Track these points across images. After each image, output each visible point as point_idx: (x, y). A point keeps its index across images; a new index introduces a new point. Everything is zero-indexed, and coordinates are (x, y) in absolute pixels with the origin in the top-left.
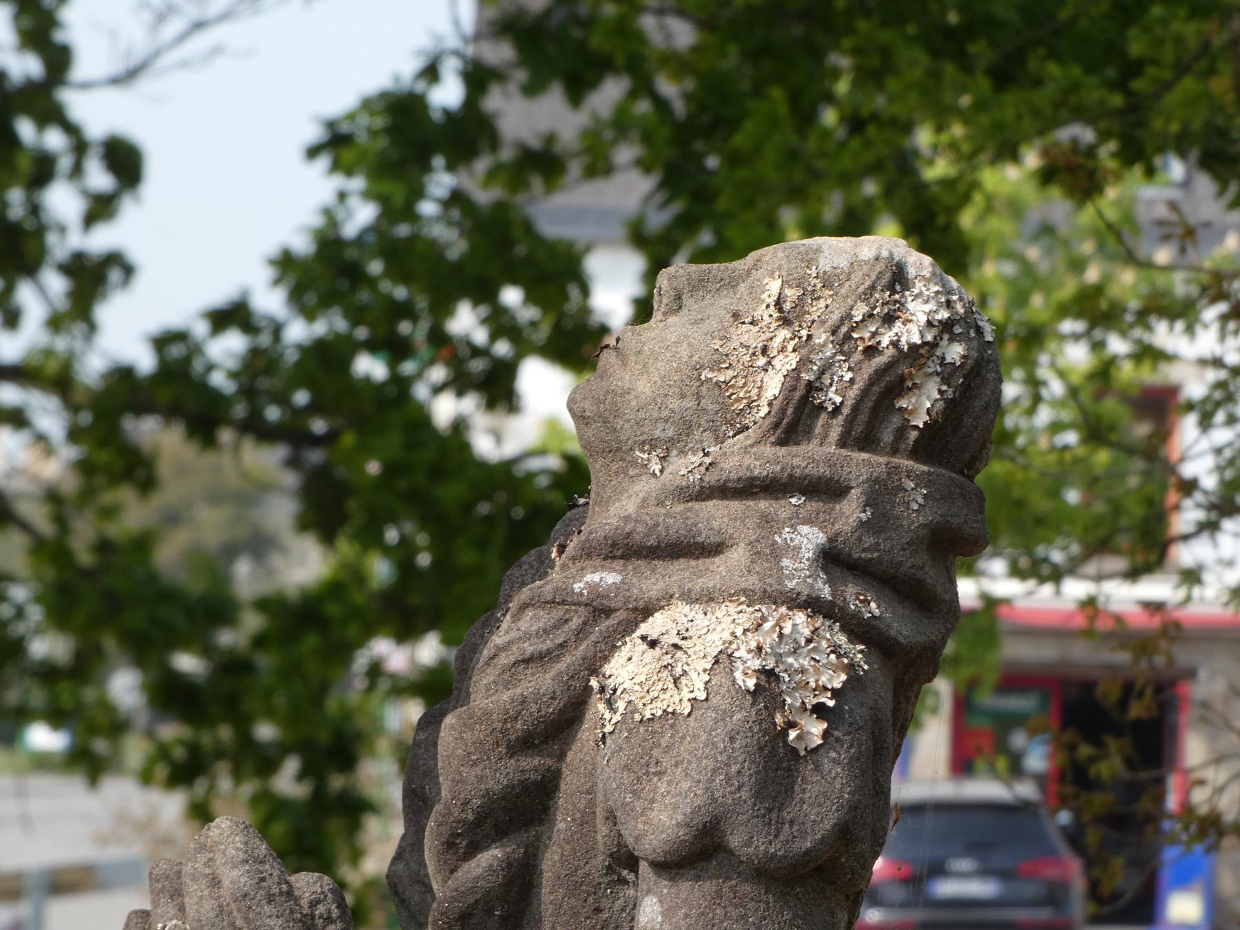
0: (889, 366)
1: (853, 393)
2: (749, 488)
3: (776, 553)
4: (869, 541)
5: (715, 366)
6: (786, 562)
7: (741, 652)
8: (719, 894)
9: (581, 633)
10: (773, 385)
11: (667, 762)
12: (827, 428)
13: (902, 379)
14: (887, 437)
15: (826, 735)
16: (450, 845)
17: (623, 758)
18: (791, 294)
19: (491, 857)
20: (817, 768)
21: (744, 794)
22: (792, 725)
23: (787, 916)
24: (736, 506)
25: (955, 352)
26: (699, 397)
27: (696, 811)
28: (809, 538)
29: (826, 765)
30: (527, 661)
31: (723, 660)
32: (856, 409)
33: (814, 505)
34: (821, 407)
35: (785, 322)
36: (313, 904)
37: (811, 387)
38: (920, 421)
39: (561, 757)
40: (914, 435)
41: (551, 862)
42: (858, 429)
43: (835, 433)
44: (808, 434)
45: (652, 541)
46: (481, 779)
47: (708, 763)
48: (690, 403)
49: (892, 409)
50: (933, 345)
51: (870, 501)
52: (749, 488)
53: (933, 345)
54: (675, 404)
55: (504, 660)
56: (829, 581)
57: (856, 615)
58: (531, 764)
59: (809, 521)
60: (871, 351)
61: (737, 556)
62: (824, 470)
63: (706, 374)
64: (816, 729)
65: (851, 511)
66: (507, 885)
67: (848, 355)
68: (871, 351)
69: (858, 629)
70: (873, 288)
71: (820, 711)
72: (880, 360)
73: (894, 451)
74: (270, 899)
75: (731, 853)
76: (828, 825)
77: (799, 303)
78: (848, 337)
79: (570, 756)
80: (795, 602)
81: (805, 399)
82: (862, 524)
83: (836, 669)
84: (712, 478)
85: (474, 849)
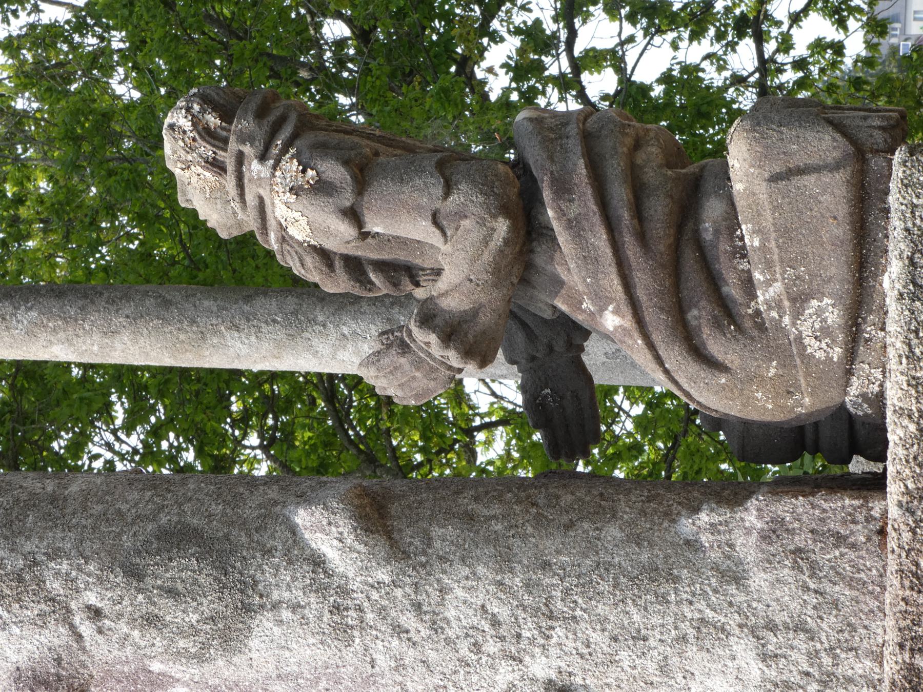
0: (199, 134)
1: (207, 146)
2: (240, 186)
3: (260, 179)
4: (257, 143)
5: (205, 193)
6: (262, 176)
7: (285, 198)
8: (368, 208)
9: (292, 247)
10: (208, 174)
11: (324, 225)
12: (220, 156)
13: (204, 128)
14: (224, 133)
15: (312, 169)
16: (370, 290)
17: (325, 239)
18: (179, 165)
19: (372, 276)
20: (324, 172)
21: (331, 201)
22: (308, 182)
23: (376, 183)
24: (247, 190)
25: (196, 107)
26: (216, 198)
27: (337, 217)
28: (255, 166)
29: (323, 169)
30: (303, 265)
31: (288, 205)
32: (214, 146)
33: (246, 163)
34: (214, 158)
35: (189, 167)
36: (383, 344)
37: (207, 162)
38: (218, 122)
39: (335, 253)
40: (223, 124)
41: (375, 256)
42: (221, 145)
43: (223, 153)
44: (223, 162)
45: (259, 221)
46: (343, 282)
47: (321, 213)
48: (218, 201)
49: (215, 132)
50: (193, 116)
51: (243, 142)
52: (240, 186)
53: (193, 116)
54: (219, 206)
55: (303, 271)
56: (268, 159)
57: (280, 151)
58: (338, 264)
59: (250, 165)
60: (194, 140)
61: (262, 192)
62: (233, 159)
63: (208, 196)
64: (310, 173)
65: (247, 149)
66: (382, 271)
67: (196, 148)
68: (194, 140)
69: (284, 151)
70: (174, 138)
71: (304, 171)
72: (197, 137)
73: (229, 131)
74: (379, 361)
75: (353, 204)
76: (342, 170)
77: (182, 162)
78: (190, 148)
79: (335, 250)
80: (273, 175)
81: (211, 164)
82: (251, 146)
83: (292, 163)
84: (237, 199)
85: (371, 282)
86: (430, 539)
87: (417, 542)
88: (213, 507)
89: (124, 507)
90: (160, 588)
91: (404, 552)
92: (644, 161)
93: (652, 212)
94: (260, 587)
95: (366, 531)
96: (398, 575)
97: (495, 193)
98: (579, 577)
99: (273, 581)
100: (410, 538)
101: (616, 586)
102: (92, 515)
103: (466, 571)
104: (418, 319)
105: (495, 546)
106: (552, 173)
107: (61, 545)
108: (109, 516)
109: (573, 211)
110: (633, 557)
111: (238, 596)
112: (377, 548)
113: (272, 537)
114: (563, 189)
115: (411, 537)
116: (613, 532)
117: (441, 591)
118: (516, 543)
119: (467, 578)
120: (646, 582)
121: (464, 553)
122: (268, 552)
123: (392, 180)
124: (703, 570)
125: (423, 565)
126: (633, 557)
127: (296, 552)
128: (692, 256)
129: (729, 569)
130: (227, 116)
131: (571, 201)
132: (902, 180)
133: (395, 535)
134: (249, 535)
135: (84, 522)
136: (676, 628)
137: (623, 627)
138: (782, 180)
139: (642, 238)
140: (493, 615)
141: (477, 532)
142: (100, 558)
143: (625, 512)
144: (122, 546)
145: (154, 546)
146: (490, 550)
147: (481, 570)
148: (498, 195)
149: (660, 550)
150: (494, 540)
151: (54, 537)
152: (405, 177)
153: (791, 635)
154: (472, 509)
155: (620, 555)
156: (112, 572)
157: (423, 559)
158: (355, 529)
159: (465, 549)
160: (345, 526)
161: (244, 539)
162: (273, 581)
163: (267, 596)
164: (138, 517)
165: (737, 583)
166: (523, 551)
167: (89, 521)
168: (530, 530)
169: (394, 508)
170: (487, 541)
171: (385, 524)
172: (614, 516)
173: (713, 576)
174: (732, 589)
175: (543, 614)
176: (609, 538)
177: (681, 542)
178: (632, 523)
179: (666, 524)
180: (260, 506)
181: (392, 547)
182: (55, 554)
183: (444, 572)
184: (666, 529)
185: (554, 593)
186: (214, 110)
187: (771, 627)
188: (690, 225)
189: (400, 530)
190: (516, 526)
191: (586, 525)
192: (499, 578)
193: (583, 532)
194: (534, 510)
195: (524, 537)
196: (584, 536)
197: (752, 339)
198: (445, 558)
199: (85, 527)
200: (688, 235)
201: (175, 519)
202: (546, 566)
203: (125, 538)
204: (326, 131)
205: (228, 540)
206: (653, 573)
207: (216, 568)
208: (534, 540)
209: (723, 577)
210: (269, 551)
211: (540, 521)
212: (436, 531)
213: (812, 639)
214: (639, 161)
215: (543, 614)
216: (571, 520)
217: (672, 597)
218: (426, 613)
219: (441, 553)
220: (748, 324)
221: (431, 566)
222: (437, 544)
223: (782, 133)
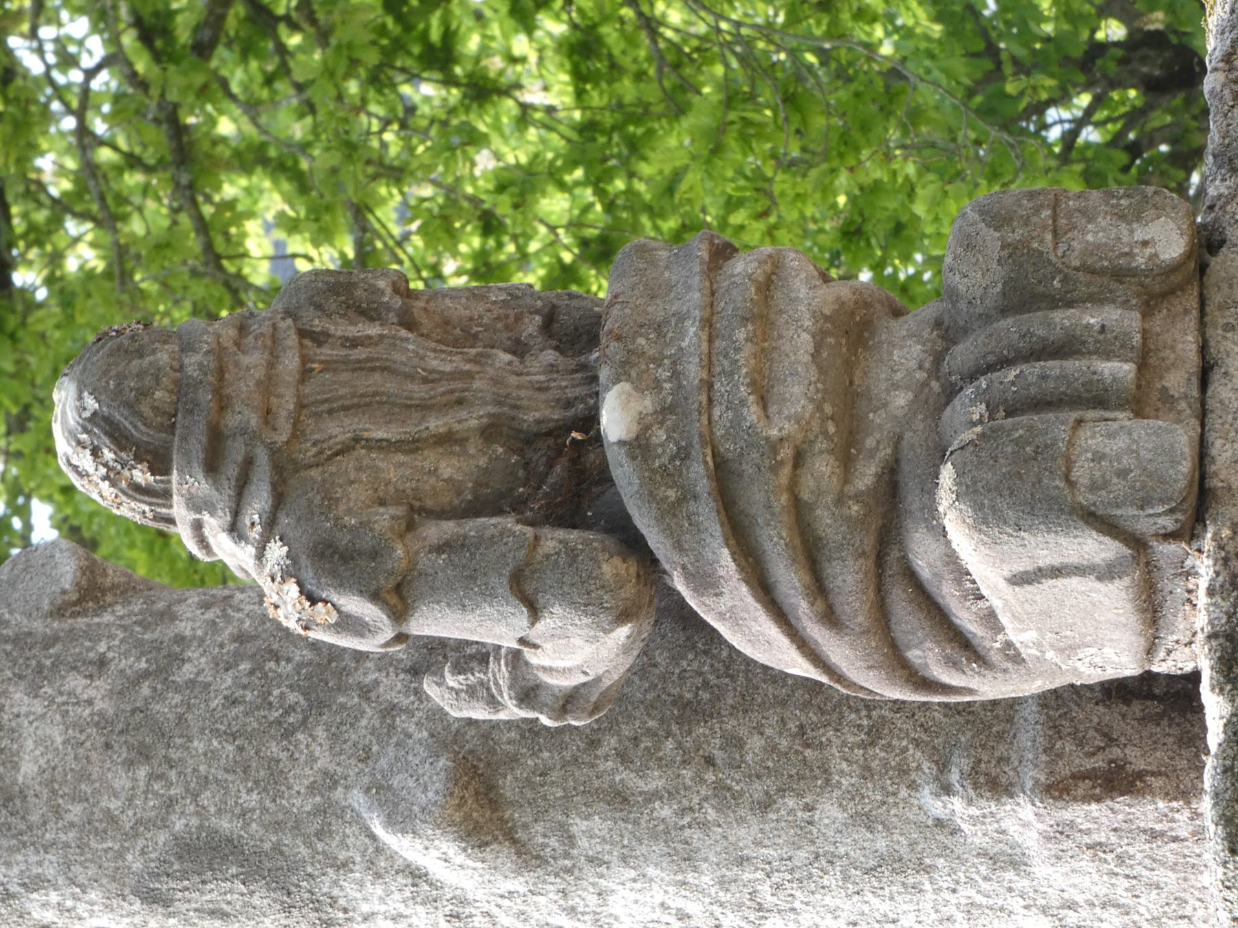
4: (220, 513)
40: (158, 478)
86: (571, 837)
87: (553, 842)
88: (244, 795)
89: (114, 805)
90: (196, 910)
91: (537, 857)
92: (812, 492)
93: (839, 582)
94: (342, 902)
95: (480, 847)
96: (535, 884)
97: (607, 608)
98: (792, 871)
99: (359, 895)
100: (539, 835)
101: (846, 879)
102: (72, 825)
103: (633, 874)
104: (513, 694)
105: (666, 842)
106: (684, 567)
107: (40, 870)
108: (97, 824)
109: (725, 602)
110: (865, 844)
111: (314, 915)
112: (499, 860)
113: (343, 844)
114: (705, 582)
115: (545, 836)
116: (830, 812)
117: (600, 894)
118: (695, 835)
119: (634, 881)
120: (886, 873)
121: (625, 851)
122: (344, 866)
123: (449, 605)
124: (965, 856)
125: (569, 871)
126: (865, 844)
127: (383, 864)
128: (904, 596)
129: (1003, 853)
130: (160, 465)
131: (720, 594)
132: (1223, 883)
133: (520, 835)
134: (310, 845)
135: (63, 838)
136: (937, 911)
137: (863, 914)
138: (1030, 583)
139: (830, 618)
140: (679, 910)
141: (636, 822)
142: (101, 885)
143: (842, 773)
144: (129, 868)
145: (176, 867)
146: (659, 847)
147: (651, 871)
148: (611, 608)
149: (901, 835)
150: (661, 832)
151: (26, 861)
152: (467, 602)
153: (1098, 910)
154: (622, 780)
155: (847, 844)
156: (124, 900)
157: (568, 863)
158: (465, 850)
159: (624, 846)
160: (450, 848)
161: (304, 851)
162: (359, 895)
163: (354, 910)
164: (139, 822)
165: (1015, 869)
166: (707, 845)
167: (71, 835)
168: (712, 814)
169: (508, 785)
170: (654, 836)
171: (501, 819)
172: (827, 781)
173: (981, 863)
174: (1010, 875)
175: (749, 908)
176: (827, 821)
177: (930, 823)
178: (855, 794)
179: (904, 793)
180: (312, 788)
181: (519, 854)
182: (35, 883)
183: (601, 876)
184: (905, 801)
185: (759, 887)
186: (138, 459)
187: (1072, 906)
188: (894, 554)
189: (525, 826)
190: (691, 809)
191: (791, 802)
192: (680, 877)
193: (788, 814)
194: (710, 777)
195: (704, 825)
196: (790, 818)
197: (1005, 671)
198: (597, 858)
199: (67, 845)
200: (892, 568)
201: (195, 822)
202: (742, 861)
203: (130, 857)
204: (317, 465)
205: (282, 853)
206: (893, 864)
207: (274, 890)
208: (720, 830)
209: (995, 863)
210: (344, 865)
211: (724, 795)
212: (579, 825)
213: (1127, 913)
214: (806, 496)
215: (749, 908)
216: (767, 793)
217: (927, 886)
218: (583, 914)
219: (591, 853)
220: (995, 657)
221: (581, 870)
222: (583, 843)
223: (1023, 539)
